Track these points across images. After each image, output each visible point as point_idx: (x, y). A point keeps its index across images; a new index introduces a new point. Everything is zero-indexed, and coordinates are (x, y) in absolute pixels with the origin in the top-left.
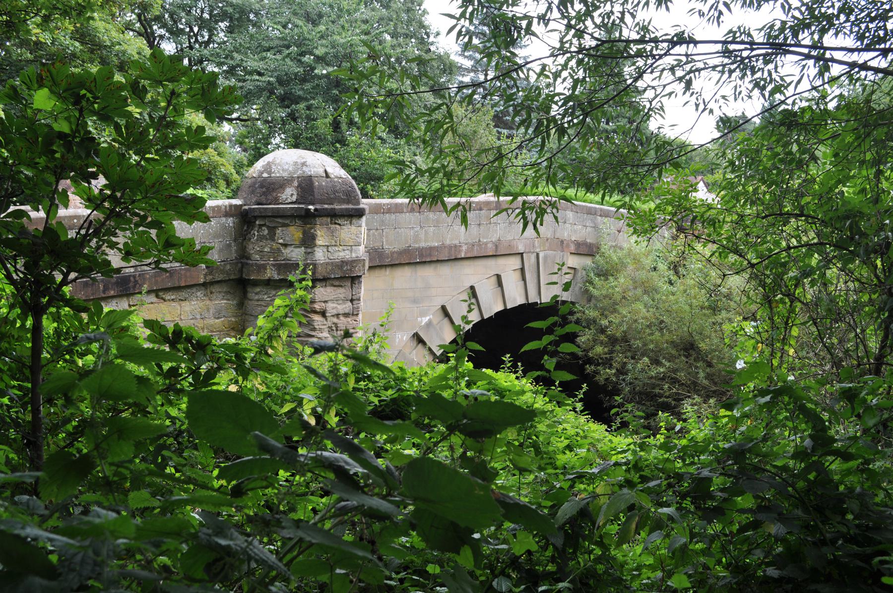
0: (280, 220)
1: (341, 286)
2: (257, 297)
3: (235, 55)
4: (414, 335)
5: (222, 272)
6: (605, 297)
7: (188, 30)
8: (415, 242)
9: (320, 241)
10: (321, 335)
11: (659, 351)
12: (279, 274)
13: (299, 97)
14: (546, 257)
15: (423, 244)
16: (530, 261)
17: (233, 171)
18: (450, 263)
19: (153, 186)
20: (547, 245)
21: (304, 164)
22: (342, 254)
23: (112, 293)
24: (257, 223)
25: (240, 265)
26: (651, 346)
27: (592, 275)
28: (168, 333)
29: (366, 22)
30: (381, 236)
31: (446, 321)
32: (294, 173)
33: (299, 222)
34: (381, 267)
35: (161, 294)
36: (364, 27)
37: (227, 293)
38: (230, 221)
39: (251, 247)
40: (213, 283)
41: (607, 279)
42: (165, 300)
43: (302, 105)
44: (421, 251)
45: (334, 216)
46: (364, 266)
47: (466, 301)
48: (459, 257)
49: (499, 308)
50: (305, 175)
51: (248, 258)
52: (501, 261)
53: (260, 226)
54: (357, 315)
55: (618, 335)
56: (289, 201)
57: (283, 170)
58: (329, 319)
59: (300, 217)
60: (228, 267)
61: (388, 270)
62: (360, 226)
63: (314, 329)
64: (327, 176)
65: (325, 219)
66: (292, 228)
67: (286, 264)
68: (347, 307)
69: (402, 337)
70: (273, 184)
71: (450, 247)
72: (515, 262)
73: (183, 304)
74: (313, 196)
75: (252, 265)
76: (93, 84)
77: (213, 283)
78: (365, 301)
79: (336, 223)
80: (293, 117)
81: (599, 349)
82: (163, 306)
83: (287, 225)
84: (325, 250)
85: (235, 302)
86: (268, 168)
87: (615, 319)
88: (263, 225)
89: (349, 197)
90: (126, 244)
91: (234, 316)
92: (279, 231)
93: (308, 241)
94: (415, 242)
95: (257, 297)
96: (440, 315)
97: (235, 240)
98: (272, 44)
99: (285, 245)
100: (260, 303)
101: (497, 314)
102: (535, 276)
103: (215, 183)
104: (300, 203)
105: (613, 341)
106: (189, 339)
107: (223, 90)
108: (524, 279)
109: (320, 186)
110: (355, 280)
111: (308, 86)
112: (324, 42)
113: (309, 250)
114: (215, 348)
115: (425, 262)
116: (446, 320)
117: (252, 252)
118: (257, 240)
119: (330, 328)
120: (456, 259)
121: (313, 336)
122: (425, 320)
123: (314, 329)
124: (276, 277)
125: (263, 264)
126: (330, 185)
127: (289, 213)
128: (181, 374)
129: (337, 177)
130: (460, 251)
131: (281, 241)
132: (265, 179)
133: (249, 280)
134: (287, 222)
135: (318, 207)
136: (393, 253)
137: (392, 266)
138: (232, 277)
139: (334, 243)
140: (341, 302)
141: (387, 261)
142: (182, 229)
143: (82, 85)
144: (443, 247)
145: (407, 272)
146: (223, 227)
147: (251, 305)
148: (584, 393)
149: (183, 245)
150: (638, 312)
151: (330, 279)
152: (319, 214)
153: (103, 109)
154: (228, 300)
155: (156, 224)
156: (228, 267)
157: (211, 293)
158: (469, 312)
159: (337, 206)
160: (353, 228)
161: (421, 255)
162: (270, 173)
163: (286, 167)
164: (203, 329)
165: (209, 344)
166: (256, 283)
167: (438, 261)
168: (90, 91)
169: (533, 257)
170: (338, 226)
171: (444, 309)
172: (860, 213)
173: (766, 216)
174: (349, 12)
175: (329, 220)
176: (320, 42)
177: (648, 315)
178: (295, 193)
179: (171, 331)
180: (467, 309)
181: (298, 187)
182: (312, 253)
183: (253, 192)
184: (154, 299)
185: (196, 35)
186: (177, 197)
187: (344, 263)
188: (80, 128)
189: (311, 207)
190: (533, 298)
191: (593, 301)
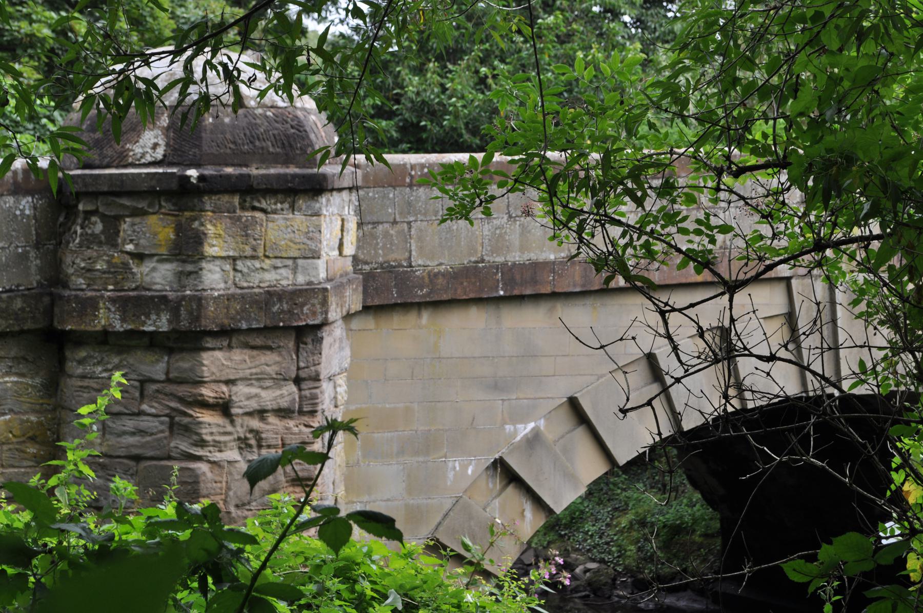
0: (126, 202)
1: (270, 348)
2: (80, 371)
8: (495, 250)
9: (213, 248)
10: (217, 456)
12: (123, 320)
15: (516, 257)
17: (463, 126)
18: (589, 301)
22: (270, 277)
25: (46, 300)
30: (406, 238)
33: (167, 206)
39: (68, 259)
44: (510, 272)
51: (66, 286)
53: (88, 214)
56: (149, 158)
58: (239, 421)
60: (18, 304)
61: (426, 316)
63: (202, 443)
65: (226, 198)
66: (153, 220)
67: (138, 298)
68: (288, 393)
69: (464, 468)
74: (199, 147)
75: (69, 300)
79: (254, 208)
83: (142, 213)
84: (228, 267)
85: (38, 380)
88: (94, 212)
91: (34, 411)
92: (125, 226)
94: (495, 250)
95: (80, 371)
96: (565, 420)
97: (37, 246)
99: (140, 257)
100: (86, 383)
104: (171, 164)
113: (189, 268)
116: (580, 434)
118: (81, 245)
121: (199, 458)
122: (525, 429)
123: (202, 443)
124: (118, 326)
125: (91, 298)
126: (243, 122)
127: (144, 187)
131: (130, 247)
134: (142, 204)
135: (209, 171)
136: (433, 276)
137: (437, 305)
138: (28, 325)
139: (248, 251)
140: (268, 383)
141: (421, 294)
151: (239, 331)
156: (18, 304)
159: (254, 171)
160: (299, 219)
161: (509, 281)
167: (555, 296)
170: (258, 215)
171: (573, 403)
175: (236, 200)
178: (162, 142)
181: (168, 129)
182: (197, 273)
187: (272, 295)
189: (193, 173)
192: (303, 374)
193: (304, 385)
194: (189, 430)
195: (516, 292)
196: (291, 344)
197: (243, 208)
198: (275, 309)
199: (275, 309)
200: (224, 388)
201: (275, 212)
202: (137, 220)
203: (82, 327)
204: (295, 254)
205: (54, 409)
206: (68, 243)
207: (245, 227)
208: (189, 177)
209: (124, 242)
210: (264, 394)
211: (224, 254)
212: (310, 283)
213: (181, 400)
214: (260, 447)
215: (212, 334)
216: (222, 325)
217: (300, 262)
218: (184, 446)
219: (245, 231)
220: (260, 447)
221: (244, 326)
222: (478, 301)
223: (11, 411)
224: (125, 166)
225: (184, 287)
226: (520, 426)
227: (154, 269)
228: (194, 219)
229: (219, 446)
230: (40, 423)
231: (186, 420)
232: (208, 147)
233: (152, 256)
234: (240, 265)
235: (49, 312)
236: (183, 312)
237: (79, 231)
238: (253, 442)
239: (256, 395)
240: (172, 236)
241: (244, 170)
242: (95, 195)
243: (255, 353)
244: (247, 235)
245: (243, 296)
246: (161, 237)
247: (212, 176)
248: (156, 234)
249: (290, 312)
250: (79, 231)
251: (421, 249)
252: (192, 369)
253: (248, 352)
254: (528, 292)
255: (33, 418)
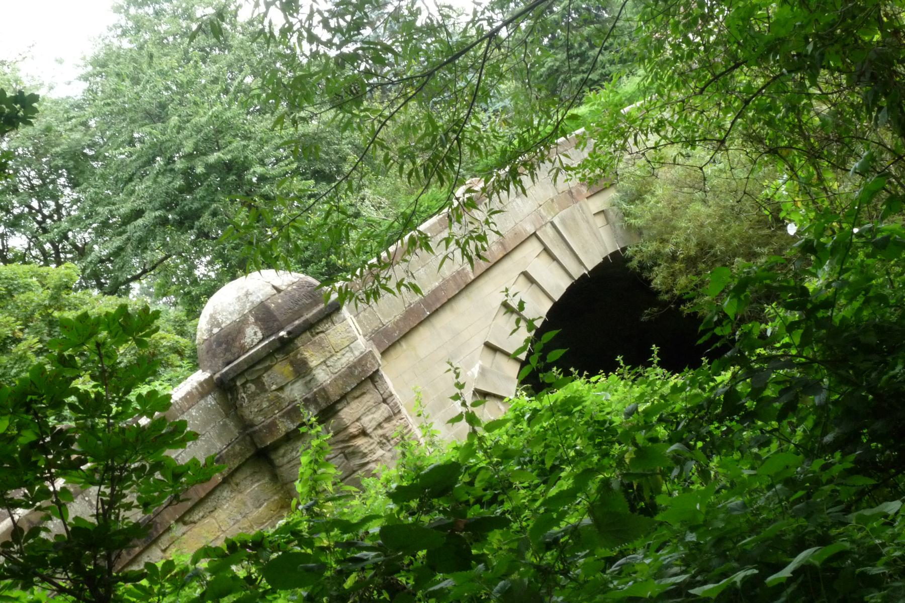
0: (259, 367)
1: (364, 393)
2: (286, 460)
3: (100, 209)
4: (474, 394)
5: (235, 456)
6: (654, 219)
7: (26, 210)
9: (313, 362)
10: (375, 457)
11: (747, 241)
12: (293, 422)
13: (197, 210)
14: (563, 221)
16: (548, 235)
17: (177, 338)
18: (464, 294)
19: (137, 440)
20: (556, 206)
21: (247, 294)
22: (344, 360)
23: (137, 550)
24: (238, 384)
25: (248, 438)
26: (736, 242)
27: (624, 206)
28: (223, 551)
29: (215, 81)
31: (499, 357)
32: (244, 310)
33: (279, 357)
34: (393, 345)
35: (187, 519)
36: (218, 88)
37: (253, 474)
38: (210, 400)
39: (247, 412)
40: (232, 474)
41: (643, 201)
42: (195, 523)
43: (206, 218)
45: (310, 327)
46: (374, 358)
47: (450, 370)
48: (470, 281)
49: (547, 306)
50: (256, 304)
51: (252, 425)
52: (517, 256)
53: (244, 385)
54: (399, 412)
55: (692, 253)
56: (256, 341)
57: (230, 314)
58: (373, 435)
59: (278, 350)
60: (237, 448)
61: (404, 344)
62: (345, 319)
63: (365, 455)
64: (279, 290)
65: (304, 336)
68: (384, 410)
70: (229, 334)
71: (454, 277)
72: (533, 247)
73: (216, 514)
74: (277, 320)
75: (260, 430)
76: (33, 388)
77: (232, 474)
78: (399, 391)
79: (318, 333)
80: (203, 234)
81: (682, 281)
82: (196, 529)
84: (324, 367)
85: (267, 479)
86: (214, 322)
87: (677, 238)
88: (247, 382)
89: (313, 296)
90: (139, 498)
91: (275, 494)
92: (266, 378)
93: (302, 370)
95: (286, 460)
96: (489, 354)
98: (130, 170)
99: (281, 389)
101: (549, 314)
102: (564, 247)
103: (167, 362)
104: (269, 337)
105: (691, 262)
106: (244, 545)
107: (139, 316)
108: (554, 258)
109: (278, 305)
110: (374, 378)
111: (200, 192)
112: (185, 132)
113: (308, 378)
114: (270, 539)
115: (437, 311)
117: (251, 417)
119: (380, 443)
120: (468, 285)
121: (368, 463)
122: (476, 370)
127: (264, 354)
128: (256, 579)
129: (289, 286)
130: (466, 275)
131: (274, 387)
132: (218, 334)
133: (267, 447)
134: (267, 363)
135: (289, 328)
136: (396, 323)
137: (405, 336)
138: (248, 455)
139: (328, 355)
140: (374, 410)
141: (397, 335)
142: (179, 456)
143: (25, 394)
144: (446, 282)
145: (424, 333)
146: (207, 410)
147: (284, 472)
148: (658, 355)
149: (189, 469)
150: (698, 214)
152: (294, 335)
153: (52, 399)
154: (258, 481)
155: (157, 466)
156: (237, 448)
157: (237, 485)
158: (457, 377)
159: (308, 315)
160: (338, 326)
161: (428, 306)
162: (218, 325)
163: (231, 309)
164: (251, 527)
165: (263, 538)
166: (275, 446)
167: (449, 300)
168: (34, 394)
169: (549, 229)
170: (322, 335)
171: (489, 346)
172: (779, 39)
173: (702, 90)
174: (190, 83)
175: (308, 334)
176: (180, 136)
177: (710, 211)
178: (257, 329)
179: (225, 547)
180: (455, 375)
182: (313, 379)
183: (214, 356)
184: (184, 528)
185: (40, 211)
186: (162, 435)
187: (351, 368)
188: (44, 429)
189: (283, 333)
190: (577, 272)
191: (645, 232)
192: (385, 396)
193: (389, 401)
194: (356, 453)
195: (434, 309)
196: (371, 386)
197: (313, 336)
198: (356, 373)
199: (356, 373)
200: (358, 424)
201: (327, 330)
202: (269, 372)
203: (275, 438)
204: (348, 343)
205: (282, 487)
206: (241, 405)
207: (320, 344)
208: (282, 337)
209: (270, 387)
210: (375, 416)
211: (319, 362)
212: (362, 353)
213: (343, 441)
214: (389, 441)
215: (338, 402)
216: (340, 395)
217: (351, 345)
218: (358, 462)
219: (320, 346)
220: (389, 441)
221: (349, 389)
222: (421, 323)
223: (265, 500)
224: (247, 352)
225: (311, 389)
226: (473, 370)
227: (292, 390)
228: (296, 354)
229: (372, 452)
230: (281, 498)
231: (351, 449)
232: (281, 318)
233: (287, 384)
234: (329, 363)
235: (253, 443)
236: (319, 400)
237: (244, 396)
238: (384, 441)
239: (373, 418)
240: (291, 369)
241: (303, 319)
242: (241, 374)
243: (360, 399)
244: (323, 348)
245: (340, 376)
246: (286, 372)
247: (293, 329)
248: (282, 373)
249: (363, 370)
250: (244, 396)
251: (383, 314)
252: (339, 424)
253: (356, 401)
254: (439, 306)
255: (276, 497)
